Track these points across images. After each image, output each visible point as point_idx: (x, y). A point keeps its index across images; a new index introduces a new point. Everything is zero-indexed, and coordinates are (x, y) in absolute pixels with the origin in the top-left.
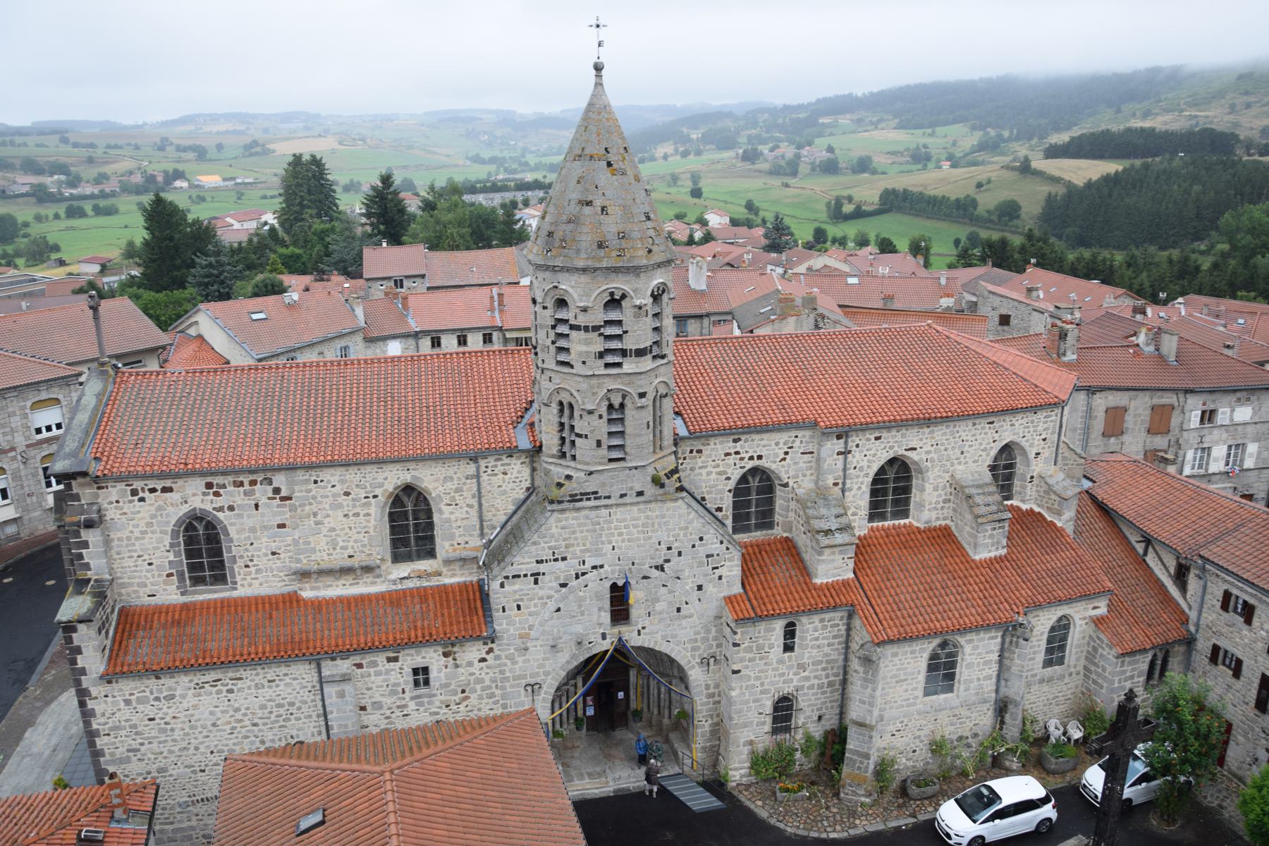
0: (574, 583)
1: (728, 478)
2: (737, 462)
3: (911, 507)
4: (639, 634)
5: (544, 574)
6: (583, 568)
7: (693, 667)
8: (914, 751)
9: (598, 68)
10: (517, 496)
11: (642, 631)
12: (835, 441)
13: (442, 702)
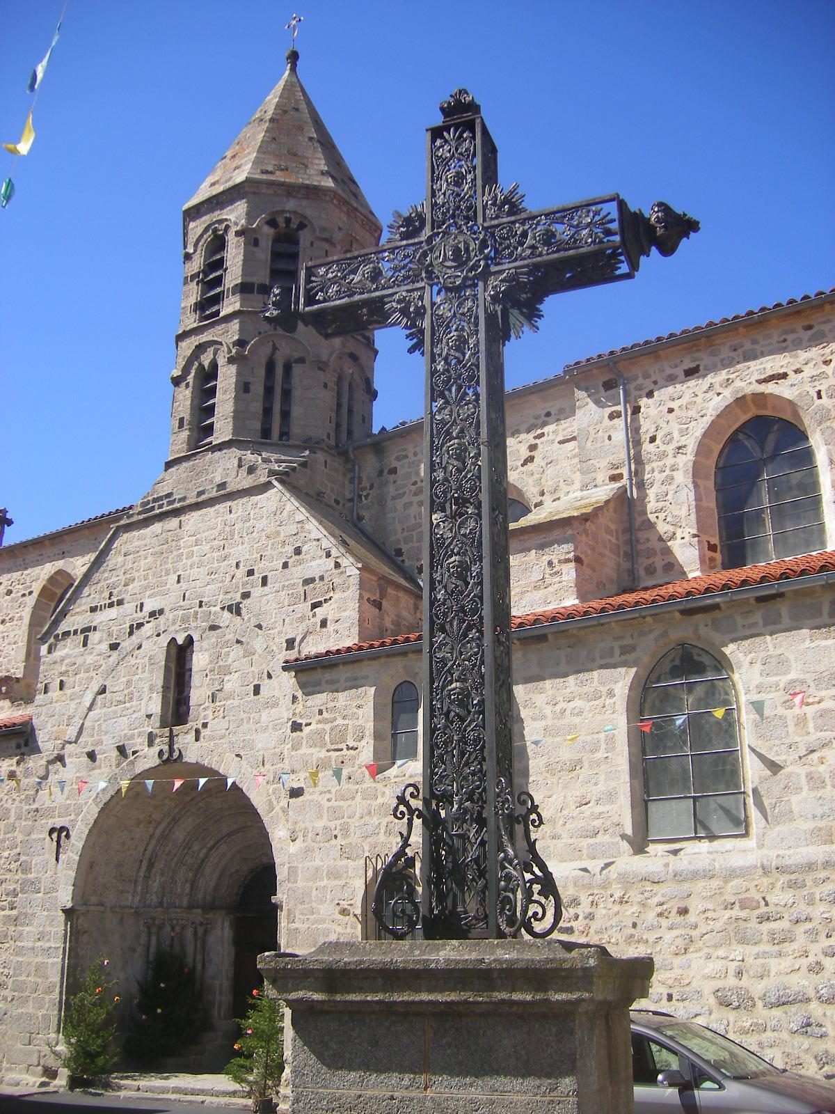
4: (197, 739)
5: (95, 629)
11: (204, 732)
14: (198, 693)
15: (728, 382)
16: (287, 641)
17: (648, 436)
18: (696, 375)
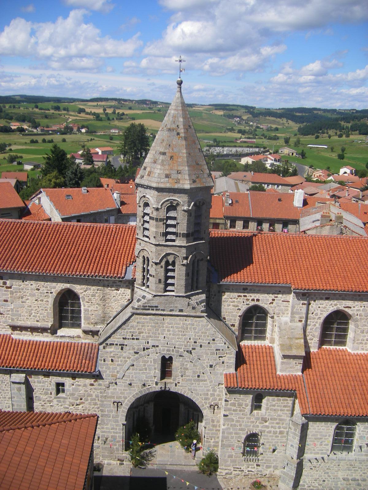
0: (142, 353)
1: (239, 309)
2: (245, 301)
3: (347, 340)
6: (147, 346)
7: (205, 409)
8: (324, 481)
9: (180, 83)
10: (123, 303)
11: (178, 384)
13: (70, 403)
15: (336, 305)
17: (311, 313)
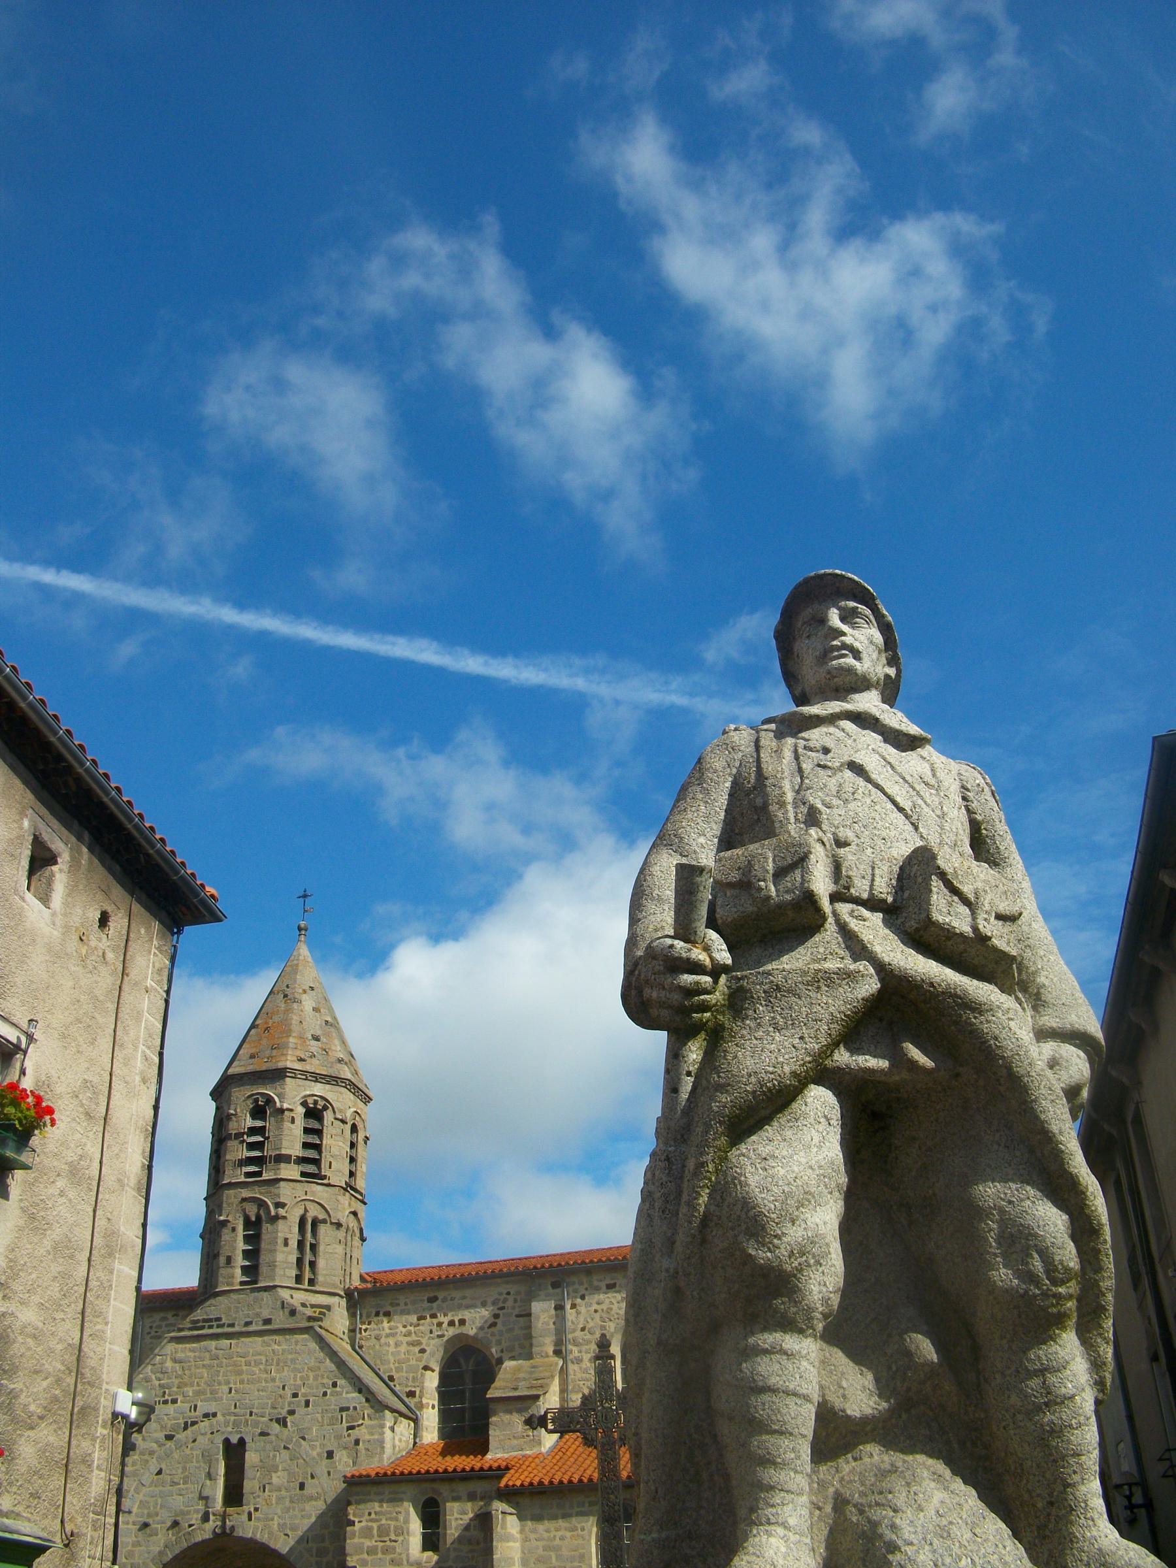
0: (181, 1436)
4: (250, 1519)
12: (550, 1290)
14: (249, 1485)
16: (328, 1452)
18: (614, 1290)
